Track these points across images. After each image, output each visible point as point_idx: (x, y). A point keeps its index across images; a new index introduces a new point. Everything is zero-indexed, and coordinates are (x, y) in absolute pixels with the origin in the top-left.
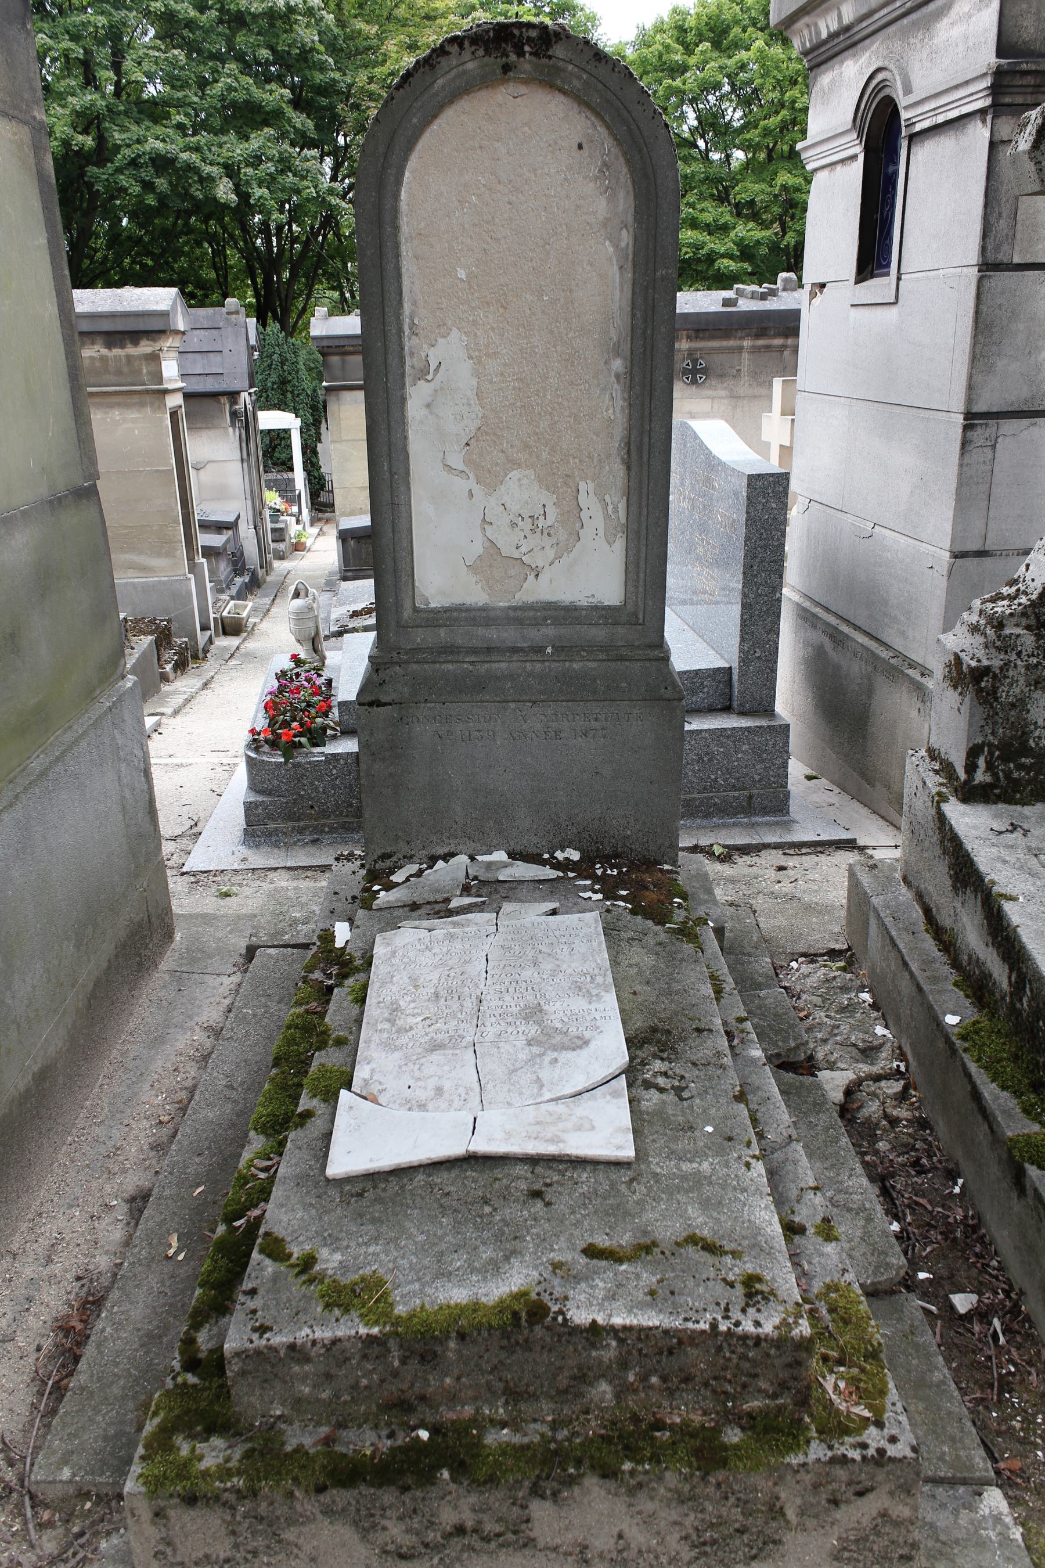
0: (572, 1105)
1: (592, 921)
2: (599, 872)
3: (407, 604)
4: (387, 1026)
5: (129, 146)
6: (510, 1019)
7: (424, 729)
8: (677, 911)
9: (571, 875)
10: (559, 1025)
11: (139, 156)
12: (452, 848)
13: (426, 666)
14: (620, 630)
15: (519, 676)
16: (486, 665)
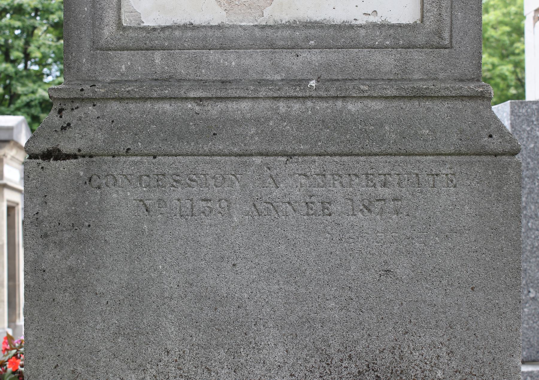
3: (110, 17)
5: (26, 95)
7: (122, 198)
11: (32, 101)
13: (132, 106)
14: (416, 55)
15: (268, 119)
16: (221, 106)
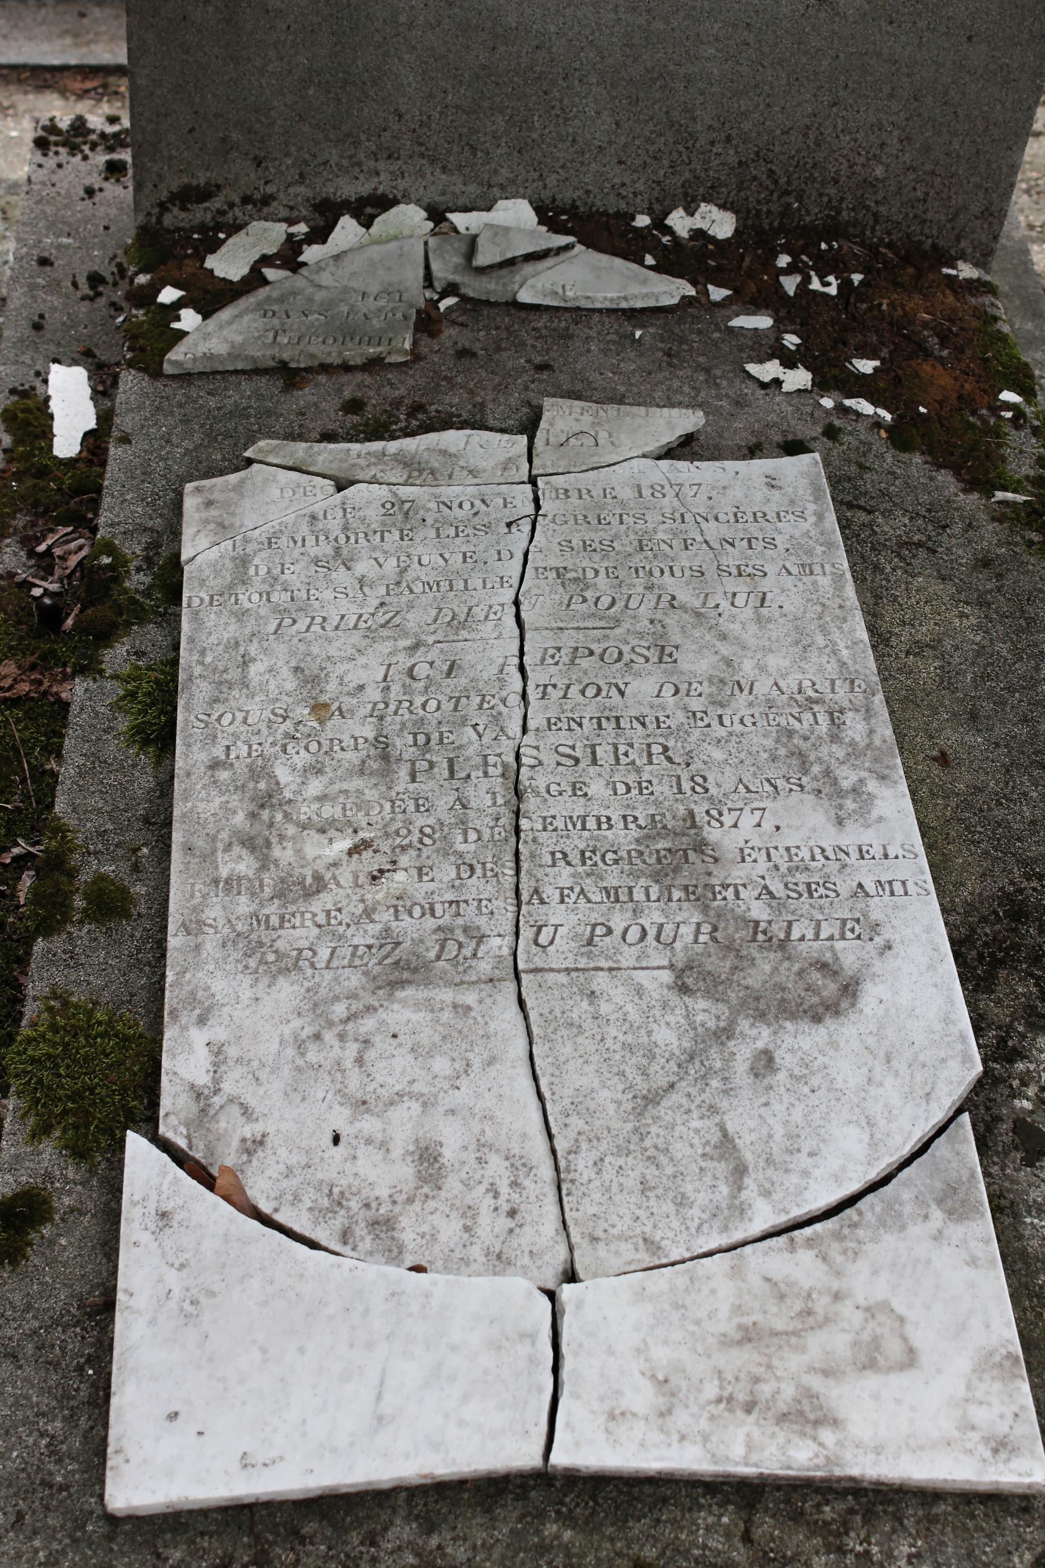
0: (834, 1249)
1: (803, 490)
2: (790, 284)
4: (244, 865)
6: (613, 878)
8: (1016, 438)
9: (717, 293)
10: (759, 911)
12: (383, 185)
